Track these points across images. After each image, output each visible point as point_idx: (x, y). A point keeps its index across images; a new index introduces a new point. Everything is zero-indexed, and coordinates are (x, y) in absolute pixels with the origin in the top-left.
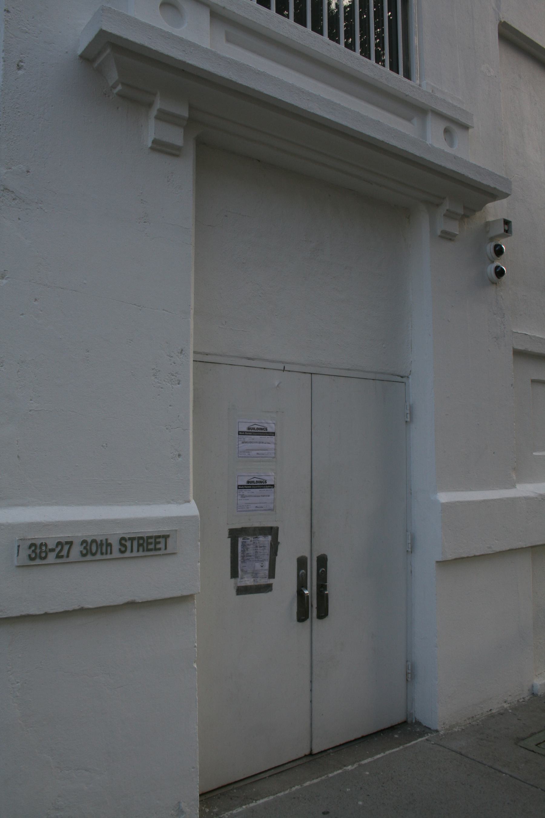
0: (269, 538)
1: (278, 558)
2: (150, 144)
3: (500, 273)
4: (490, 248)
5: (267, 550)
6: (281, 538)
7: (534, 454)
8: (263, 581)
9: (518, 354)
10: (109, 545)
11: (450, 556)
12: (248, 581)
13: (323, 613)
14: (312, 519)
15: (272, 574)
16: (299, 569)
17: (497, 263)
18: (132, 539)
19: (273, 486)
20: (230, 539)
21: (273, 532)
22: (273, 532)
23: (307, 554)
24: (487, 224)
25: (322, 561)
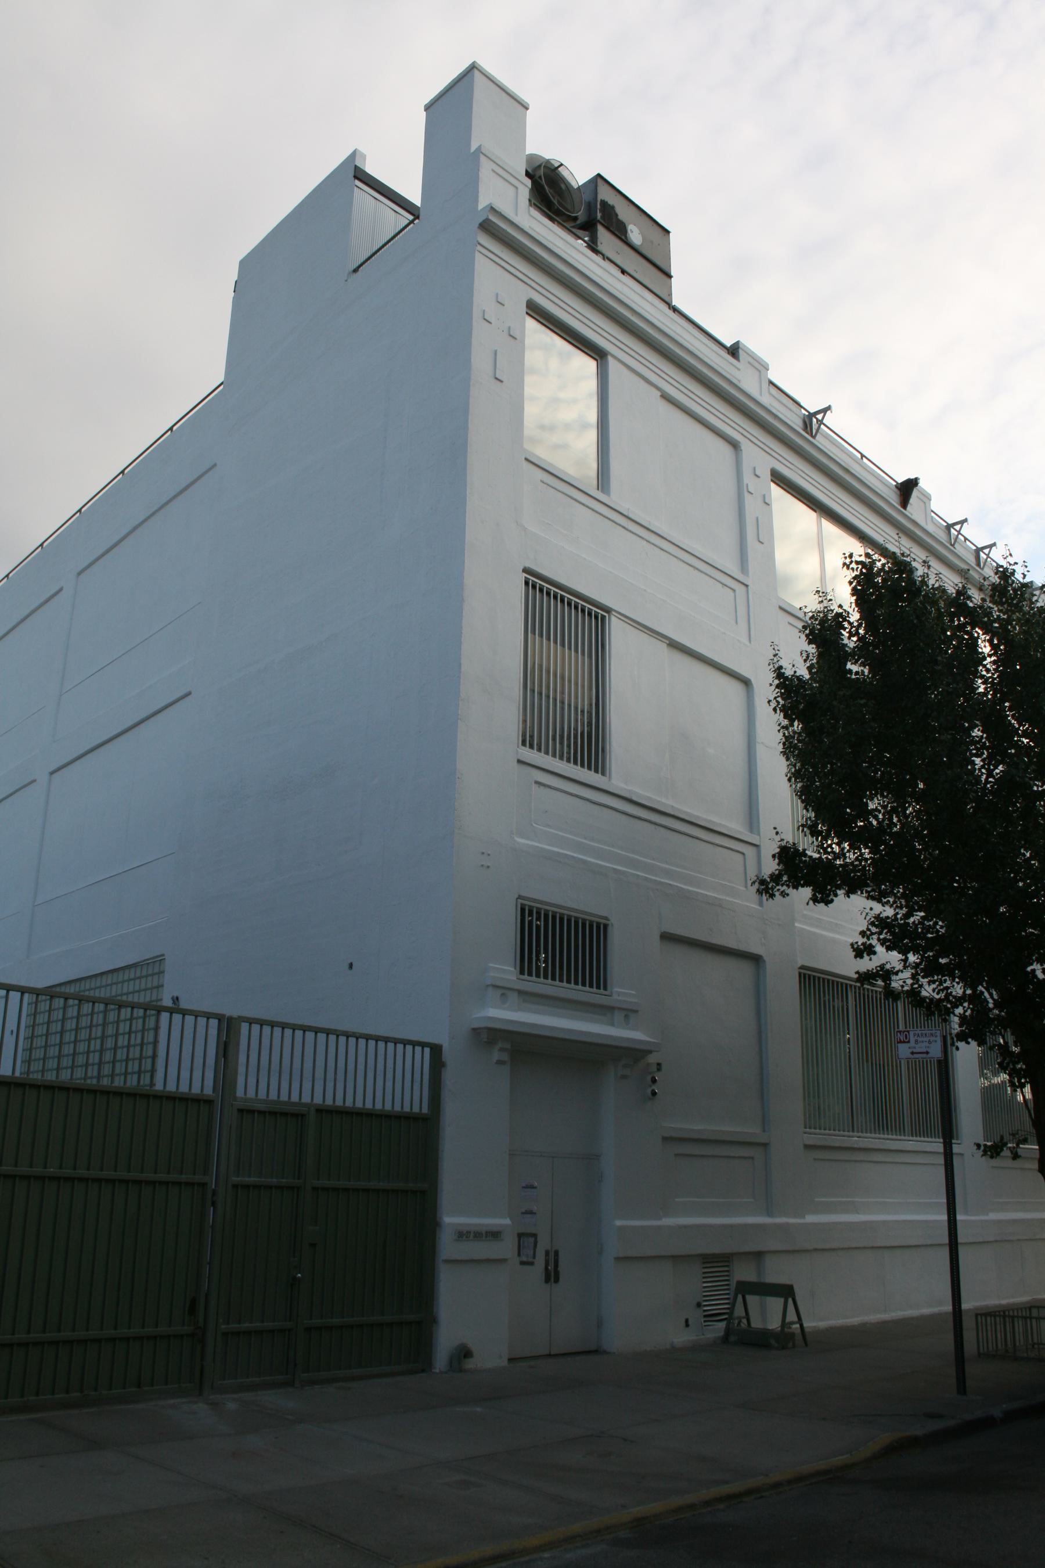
0: (533, 1239)
1: (537, 1250)
2: (495, 1061)
3: (654, 1093)
4: (649, 1078)
5: (533, 1244)
6: (538, 1239)
7: (677, 1200)
8: (531, 1260)
9: (666, 1139)
10: (482, 1234)
11: (621, 1255)
12: (524, 1259)
13: (557, 1280)
14: (612, 264)
15: (534, 1257)
16: (546, 1256)
17: (653, 1087)
18: (489, 1232)
19: (535, 1213)
20: (806, 1216)
21: (535, 1236)
22: (535, 1236)
23: (549, 1248)
24: (648, 1064)
25: (556, 1253)
